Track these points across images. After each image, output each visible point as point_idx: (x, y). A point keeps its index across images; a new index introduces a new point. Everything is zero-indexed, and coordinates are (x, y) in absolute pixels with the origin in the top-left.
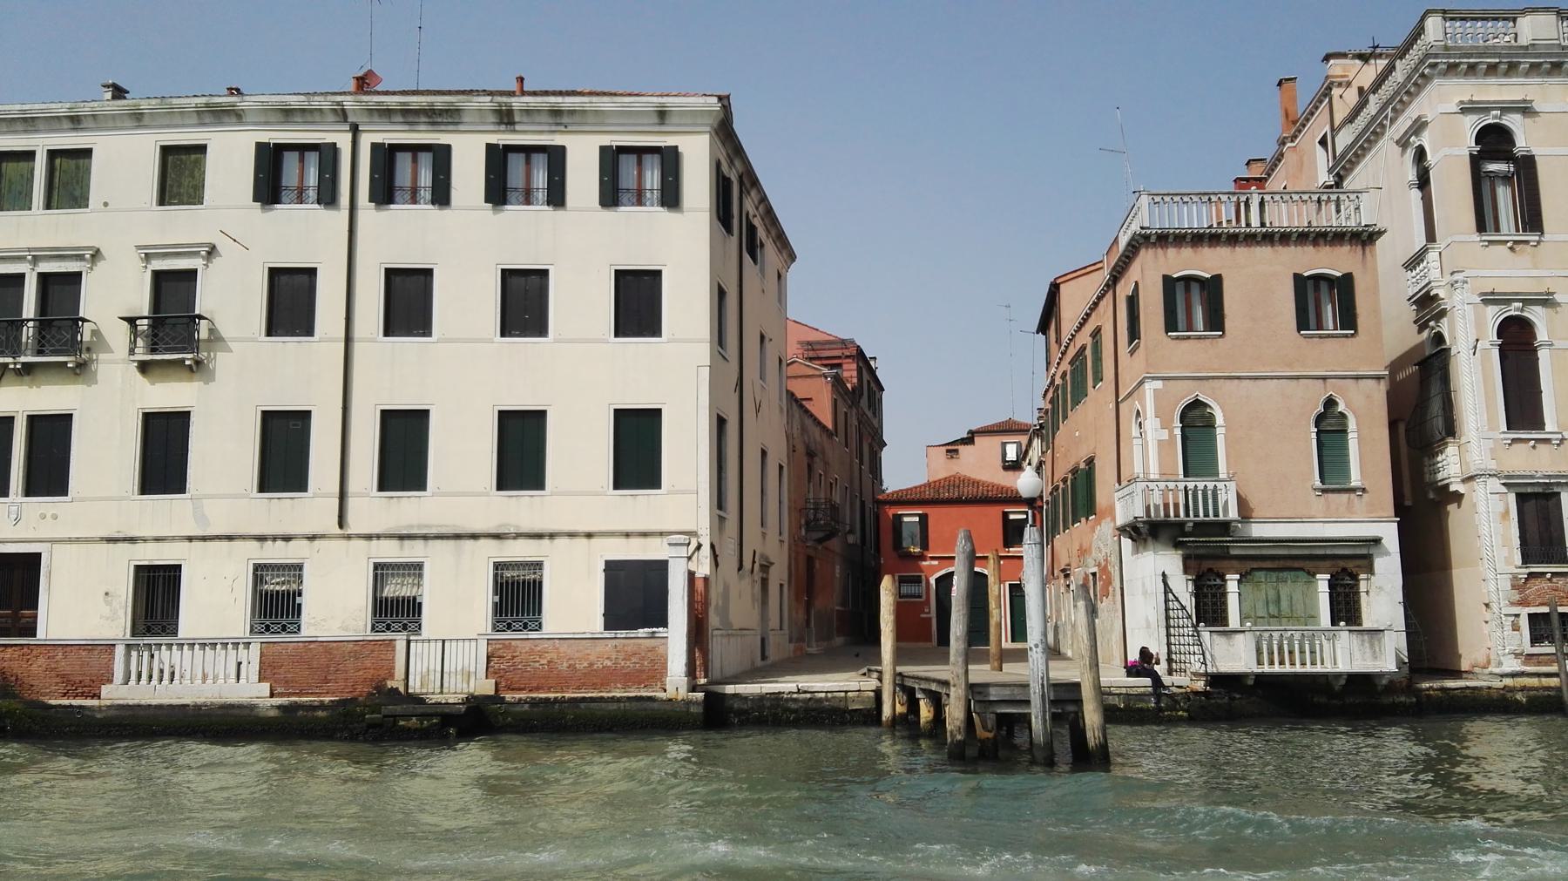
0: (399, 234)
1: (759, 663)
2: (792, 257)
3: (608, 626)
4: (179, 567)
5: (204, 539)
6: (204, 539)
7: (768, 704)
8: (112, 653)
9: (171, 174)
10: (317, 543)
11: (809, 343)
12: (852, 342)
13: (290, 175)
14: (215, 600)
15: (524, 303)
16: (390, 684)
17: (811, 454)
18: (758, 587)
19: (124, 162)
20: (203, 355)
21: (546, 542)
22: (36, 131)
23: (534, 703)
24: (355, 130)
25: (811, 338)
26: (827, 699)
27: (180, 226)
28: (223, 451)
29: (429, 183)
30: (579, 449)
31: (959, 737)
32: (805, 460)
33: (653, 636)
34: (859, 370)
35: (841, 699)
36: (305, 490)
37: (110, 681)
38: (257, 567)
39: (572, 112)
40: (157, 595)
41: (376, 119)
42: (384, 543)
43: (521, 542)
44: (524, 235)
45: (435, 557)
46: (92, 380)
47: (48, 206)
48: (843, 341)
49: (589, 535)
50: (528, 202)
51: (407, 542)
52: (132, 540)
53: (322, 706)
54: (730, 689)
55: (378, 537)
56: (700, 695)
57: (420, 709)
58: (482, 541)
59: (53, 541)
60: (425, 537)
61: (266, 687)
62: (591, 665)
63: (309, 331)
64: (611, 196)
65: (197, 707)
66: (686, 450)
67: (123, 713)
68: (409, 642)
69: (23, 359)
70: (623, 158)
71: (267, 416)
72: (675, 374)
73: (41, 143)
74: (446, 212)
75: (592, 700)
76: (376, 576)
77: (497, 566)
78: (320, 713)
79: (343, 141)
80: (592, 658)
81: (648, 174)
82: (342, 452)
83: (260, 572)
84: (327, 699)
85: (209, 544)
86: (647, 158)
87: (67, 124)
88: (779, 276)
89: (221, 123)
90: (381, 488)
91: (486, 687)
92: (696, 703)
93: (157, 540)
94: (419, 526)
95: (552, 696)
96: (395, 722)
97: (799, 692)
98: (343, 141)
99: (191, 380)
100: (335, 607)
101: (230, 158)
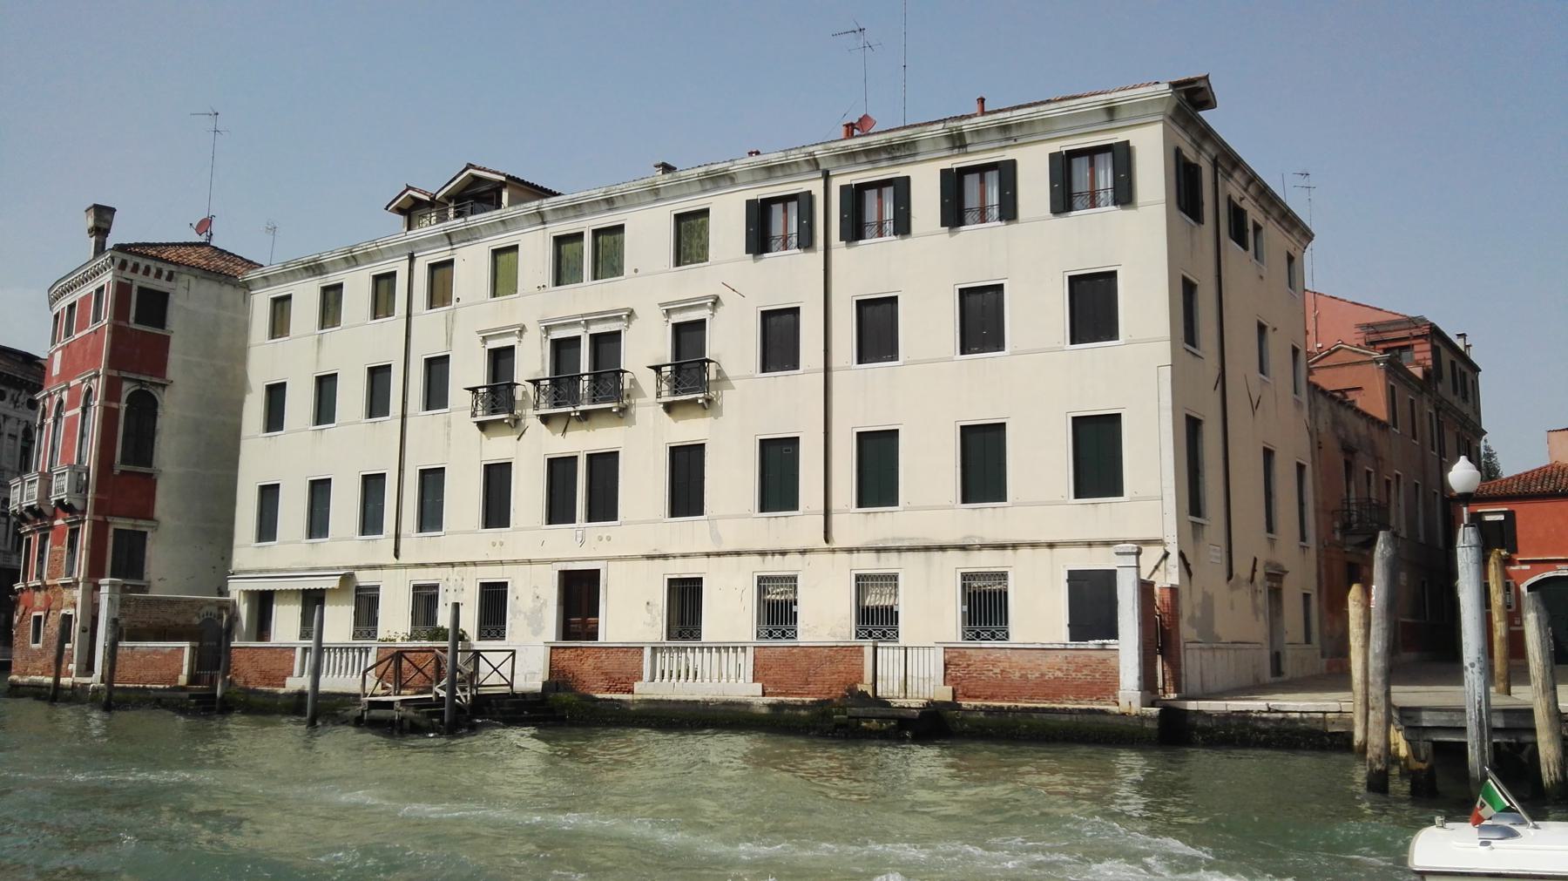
0: (866, 267)
1: (1267, 677)
2: (1307, 235)
3: (1074, 636)
4: (700, 580)
5: (718, 554)
6: (718, 554)
7: (1234, 722)
8: (642, 654)
9: (684, 239)
10: (807, 556)
11: (1369, 326)
12: (1422, 319)
13: (971, 199)
14: (729, 611)
15: (981, 318)
16: (860, 687)
17: (1349, 450)
18: (1262, 599)
19: (648, 231)
20: (712, 394)
21: (1009, 552)
22: (583, 215)
23: (989, 711)
24: (827, 176)
25: (1372, 320)
26: (1302, 720)
27: (694, 282)
28: (732, 478)
29: (996, 201)
30: (1039, 460)
31: (1378, 767)
32: (1340, 459)
33: (1103, 648)
34: (1435, 352)
35: (1318, 721)
36: (1004, 500)
37: (641, 679)
38: (761, 579)
39: (1020, 125)
40: (685, 601)
41: (844, 162)
42: (864, 556)
43: (986, 553)
44: (981, 251)
45: (908, 569)
46: (718, 413)
47: (595, 278)
48: (1411, 320)
49: (1051, 545)
50: (1093, 205)
51: (883, 555)
52: (665, 557)
53: (804, 706)
54: (1192, 705)
55: (858, 550)
56: (1155, 711)
57: (880, 711)
58: (950, 553)
59: (609, 559)
60: (899, 550)
61: (759, 686)
62: (1043, 675)
63: (795, 365)
64: (1063, 201)
65: (706, 703)
66: (1149, 456)
67: (653, 706)
68: (875, 648)
69: (581, 408)
70: (1076, 162)
71: (764, 444)
72: (1136, 376)
73: (587, 224)
74: (908, 241)
75: (1044, 710)
76: (858, 587)
77: (965, 576)
78: (803, 713)
79: (817, 187)
80: (1044, 669)
81: (1101, 174)
82: (825, 473)
83: (764, 582)
84: (808, 699)
85: (723, 559)
86: (1100, 158)
87: (604, 206)
88: (1290, 259)
89: (718, 188)
90: (860, 504)
91: (944, 694)
92: (1151, 718)
93: (684, 556)
94: (894, 539)
95: (1005, 704)
96: (858, 725)
97: (1269, 710)
98: (817, 187)
99: (704, 416)
100: (825, 617)
101: (727, 218)
